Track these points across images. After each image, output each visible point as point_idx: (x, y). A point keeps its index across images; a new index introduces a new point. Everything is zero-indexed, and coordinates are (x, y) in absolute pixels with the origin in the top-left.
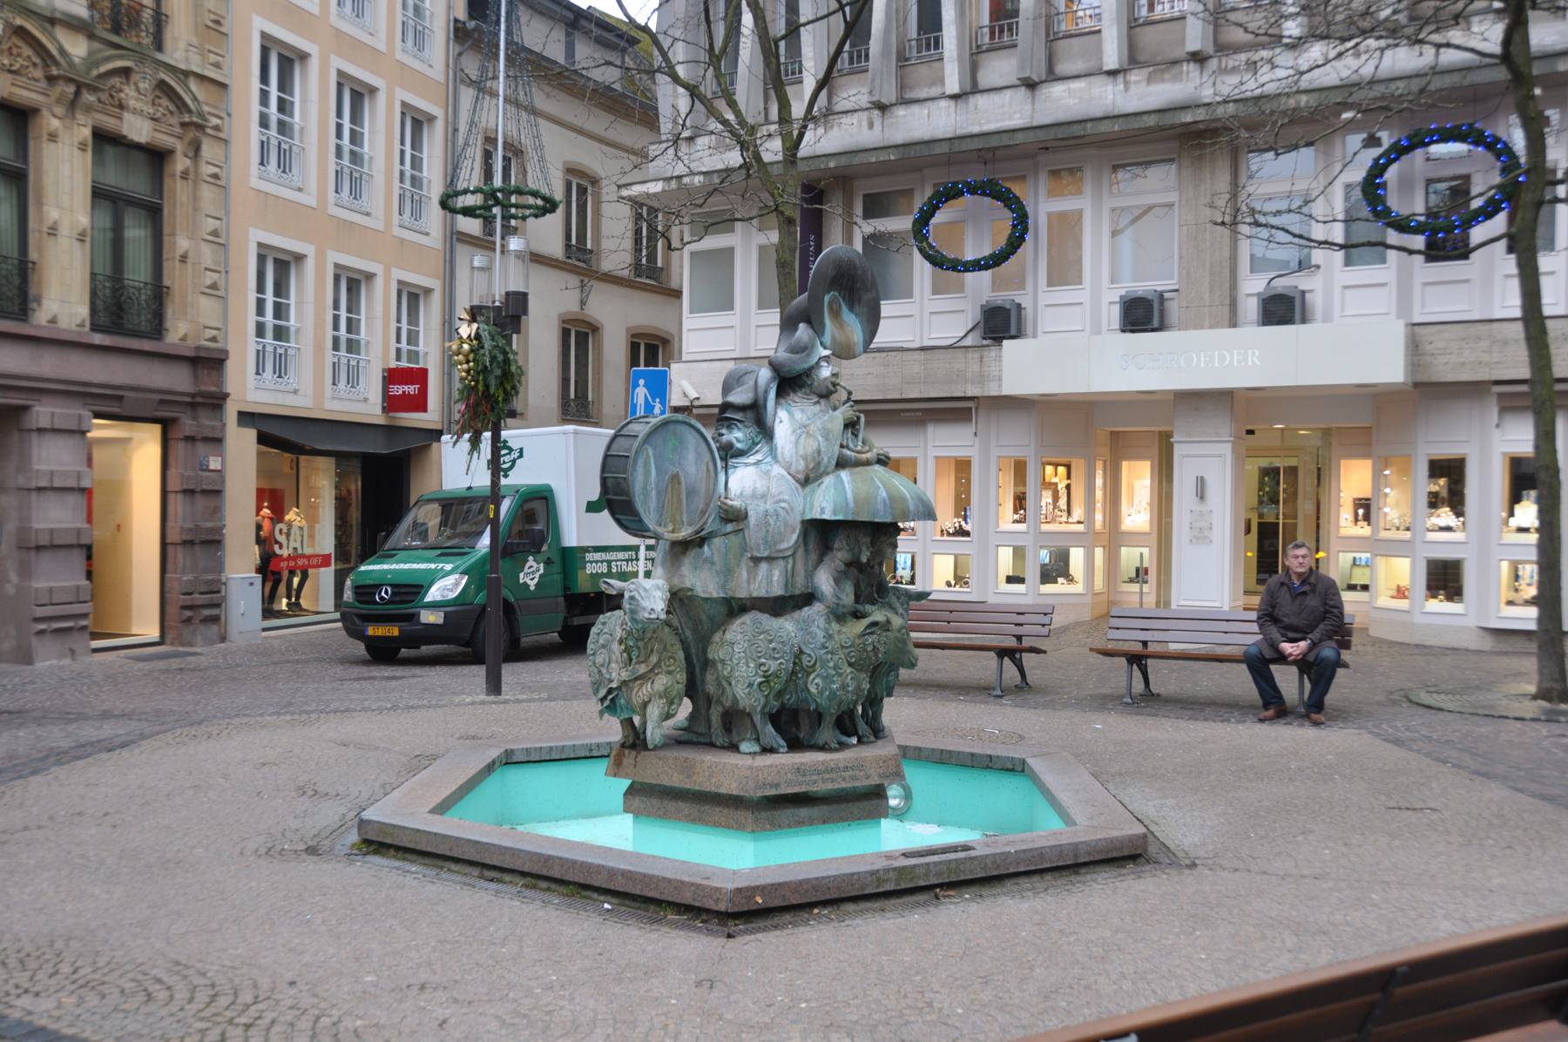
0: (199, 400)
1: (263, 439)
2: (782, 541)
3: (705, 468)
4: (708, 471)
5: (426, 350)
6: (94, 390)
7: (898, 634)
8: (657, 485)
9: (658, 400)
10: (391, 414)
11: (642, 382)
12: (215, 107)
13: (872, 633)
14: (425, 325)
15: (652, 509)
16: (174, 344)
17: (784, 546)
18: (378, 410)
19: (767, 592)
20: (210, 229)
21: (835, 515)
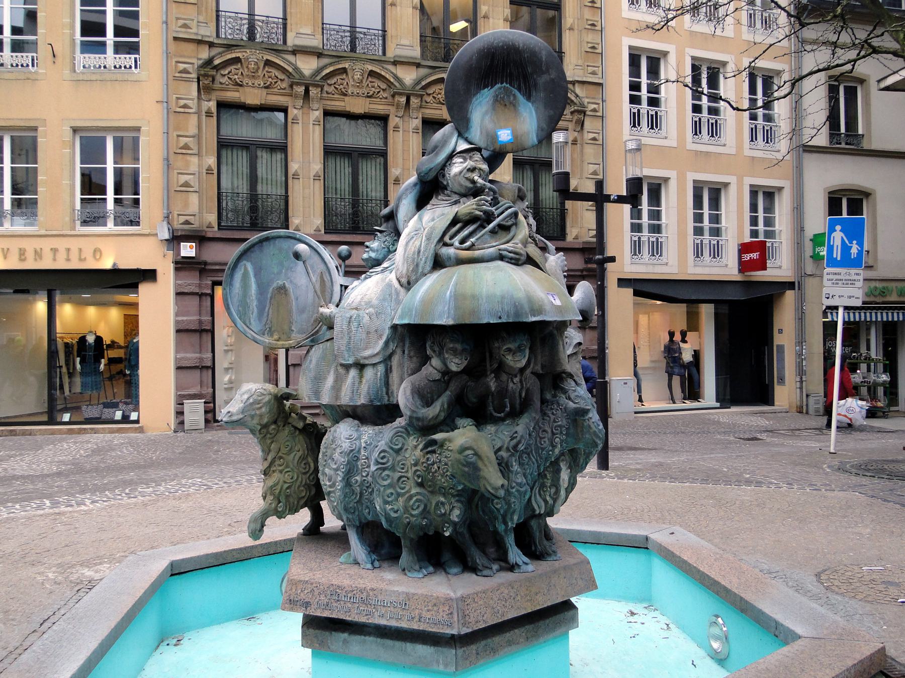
0: (585, 273)
1: (637, 293)
2: (366, 349)
5: (781, 229)
7: (457, 456)
9: (855, 242)
10: (746, 274)
11: (838, 228)
12: (593, 98)
13: (434, 452)
14: (780, 212)
16: (570, 242)
17: (367, 353)
18: (735, 271)
19: (351, 399)
20: (591, 171)
21: (402, 320)
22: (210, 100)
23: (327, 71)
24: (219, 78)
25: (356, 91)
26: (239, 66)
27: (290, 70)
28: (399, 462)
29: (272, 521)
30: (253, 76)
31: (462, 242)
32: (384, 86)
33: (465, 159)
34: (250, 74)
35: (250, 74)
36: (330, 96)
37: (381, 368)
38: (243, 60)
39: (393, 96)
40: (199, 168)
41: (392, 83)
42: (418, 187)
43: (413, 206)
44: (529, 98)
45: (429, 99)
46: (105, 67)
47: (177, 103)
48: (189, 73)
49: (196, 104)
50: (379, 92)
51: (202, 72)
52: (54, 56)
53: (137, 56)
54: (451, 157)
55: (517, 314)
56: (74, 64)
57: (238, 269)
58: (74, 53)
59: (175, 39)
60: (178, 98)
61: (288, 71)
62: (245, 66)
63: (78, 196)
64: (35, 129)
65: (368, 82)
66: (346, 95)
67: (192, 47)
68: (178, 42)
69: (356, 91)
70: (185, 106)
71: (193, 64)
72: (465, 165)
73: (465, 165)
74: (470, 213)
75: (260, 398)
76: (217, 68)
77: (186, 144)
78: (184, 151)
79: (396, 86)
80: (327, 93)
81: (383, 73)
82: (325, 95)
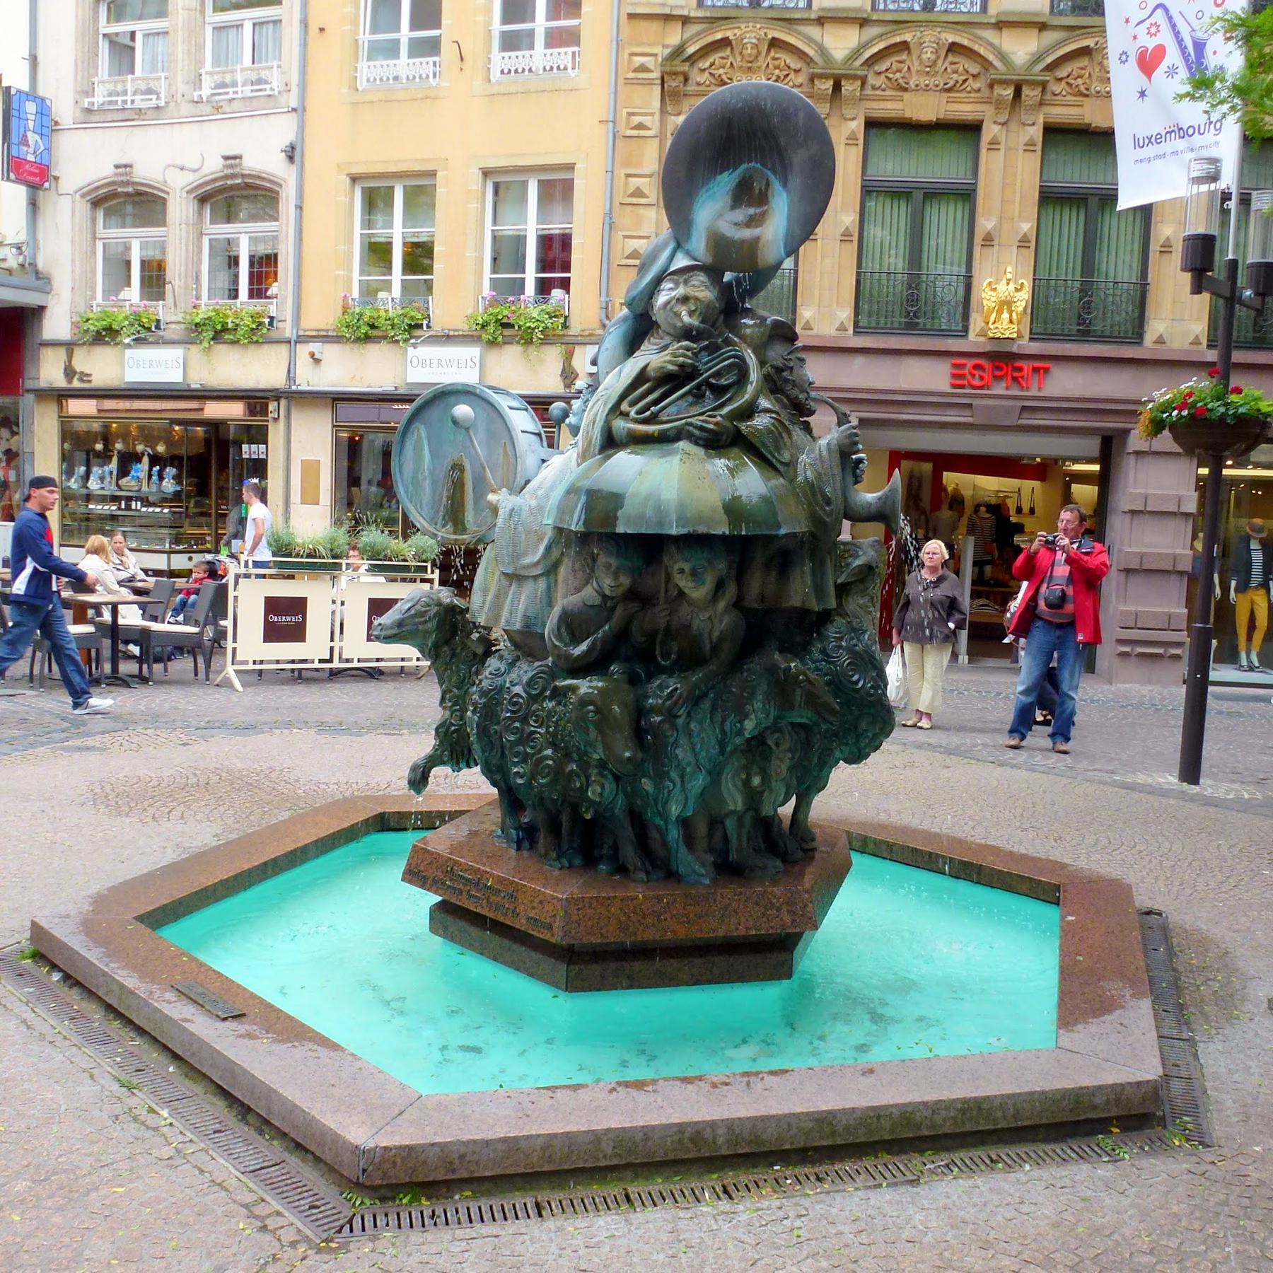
2: (525, 554)
3: (501, 451)
4: (506, 454)
6: (1108, 406)
8: (432, 472)
15: (424, 502)
17: (527, 560)
22: (679, 114)
23: (875, 50)
24: (696, 77)
25: (924, 81)
26: (728, 52)
27: (811, 53)
28: (534, 712)
29: (439, 773)
30: (750, 68)
31: (638, 413)
32: (974, 69)
33: (677, 284)
34: (745, 65)
35: (745, 65)
36: (878, 92)
37: (542, 584)
38: (734, 42)
39: (991, 86)
40: (657, 227)
41: (991, 64)
42: (630, 322)
43: (621, 350)
44: (785, 184)
45: (1057, 88)
46: (530, 70)
47: (628, 121)
48: (649, 71)
49: (657, 123)
50: (965, 81)
51: (668, 69)
52: (462, 59)
53: (576, 49)
54: (658, 281)
55: (660, 523)
56: (489, 69)
57: (409, 435)
58: (489, 52)
59: (631, 16)
60: (630, 114)
61: (806, 55)
62: (737, 52)
63: (487, 274)
64: (433, 174)
65: (947, 64)
66: (905, 90)
67: (654, 26)
68: (636, 22)
69: (924, 81)
70: (640, 126)
71: (655, 55)
72: (674, 293)
73: (674, 293)
74: (661, 368)
75: (423, 609)
76: (692, 59)
77: (638, 188)
78: (635, 200)
79: (996, 68)
80: (874, 88)
81: (976, 48)
82: (868, 91)
